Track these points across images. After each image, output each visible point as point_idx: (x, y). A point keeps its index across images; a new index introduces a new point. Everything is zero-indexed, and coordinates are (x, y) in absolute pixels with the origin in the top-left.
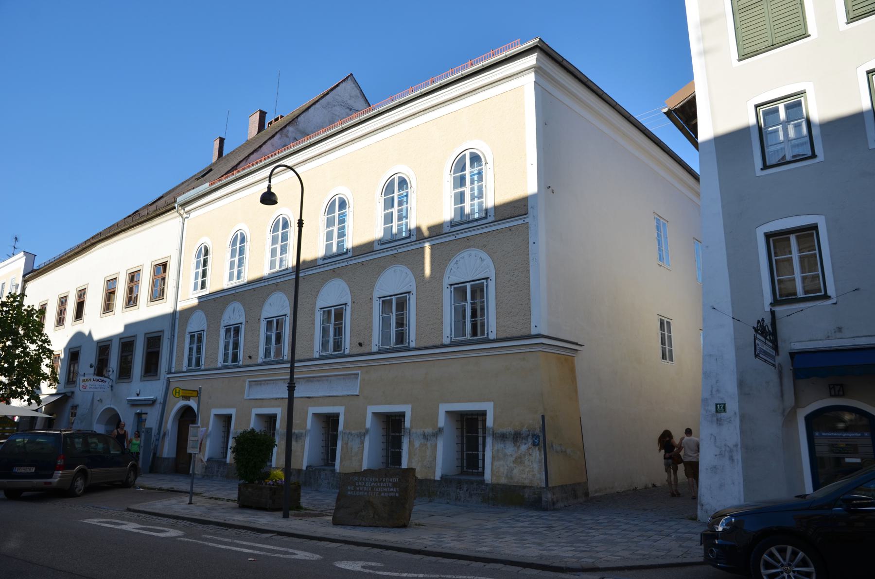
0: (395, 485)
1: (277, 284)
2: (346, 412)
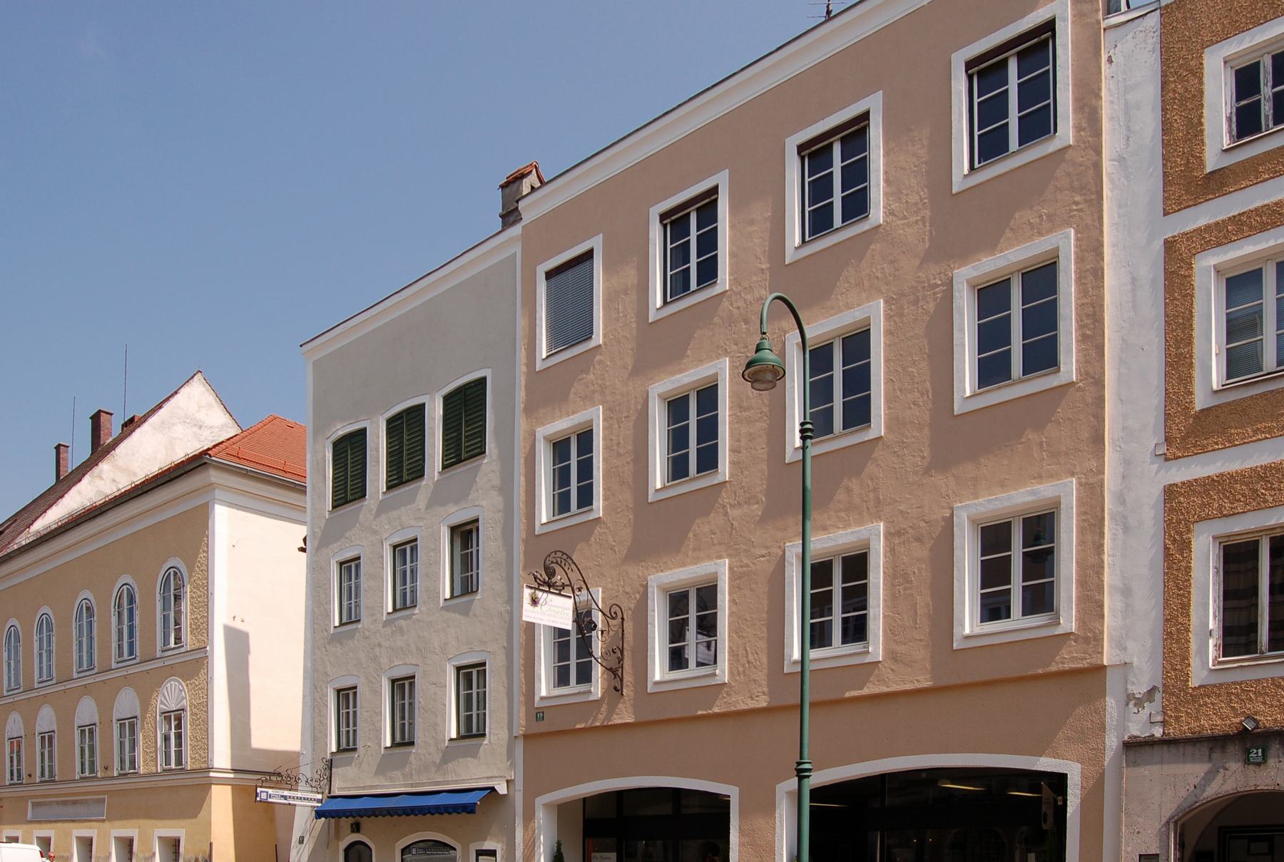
1: (45, 696)
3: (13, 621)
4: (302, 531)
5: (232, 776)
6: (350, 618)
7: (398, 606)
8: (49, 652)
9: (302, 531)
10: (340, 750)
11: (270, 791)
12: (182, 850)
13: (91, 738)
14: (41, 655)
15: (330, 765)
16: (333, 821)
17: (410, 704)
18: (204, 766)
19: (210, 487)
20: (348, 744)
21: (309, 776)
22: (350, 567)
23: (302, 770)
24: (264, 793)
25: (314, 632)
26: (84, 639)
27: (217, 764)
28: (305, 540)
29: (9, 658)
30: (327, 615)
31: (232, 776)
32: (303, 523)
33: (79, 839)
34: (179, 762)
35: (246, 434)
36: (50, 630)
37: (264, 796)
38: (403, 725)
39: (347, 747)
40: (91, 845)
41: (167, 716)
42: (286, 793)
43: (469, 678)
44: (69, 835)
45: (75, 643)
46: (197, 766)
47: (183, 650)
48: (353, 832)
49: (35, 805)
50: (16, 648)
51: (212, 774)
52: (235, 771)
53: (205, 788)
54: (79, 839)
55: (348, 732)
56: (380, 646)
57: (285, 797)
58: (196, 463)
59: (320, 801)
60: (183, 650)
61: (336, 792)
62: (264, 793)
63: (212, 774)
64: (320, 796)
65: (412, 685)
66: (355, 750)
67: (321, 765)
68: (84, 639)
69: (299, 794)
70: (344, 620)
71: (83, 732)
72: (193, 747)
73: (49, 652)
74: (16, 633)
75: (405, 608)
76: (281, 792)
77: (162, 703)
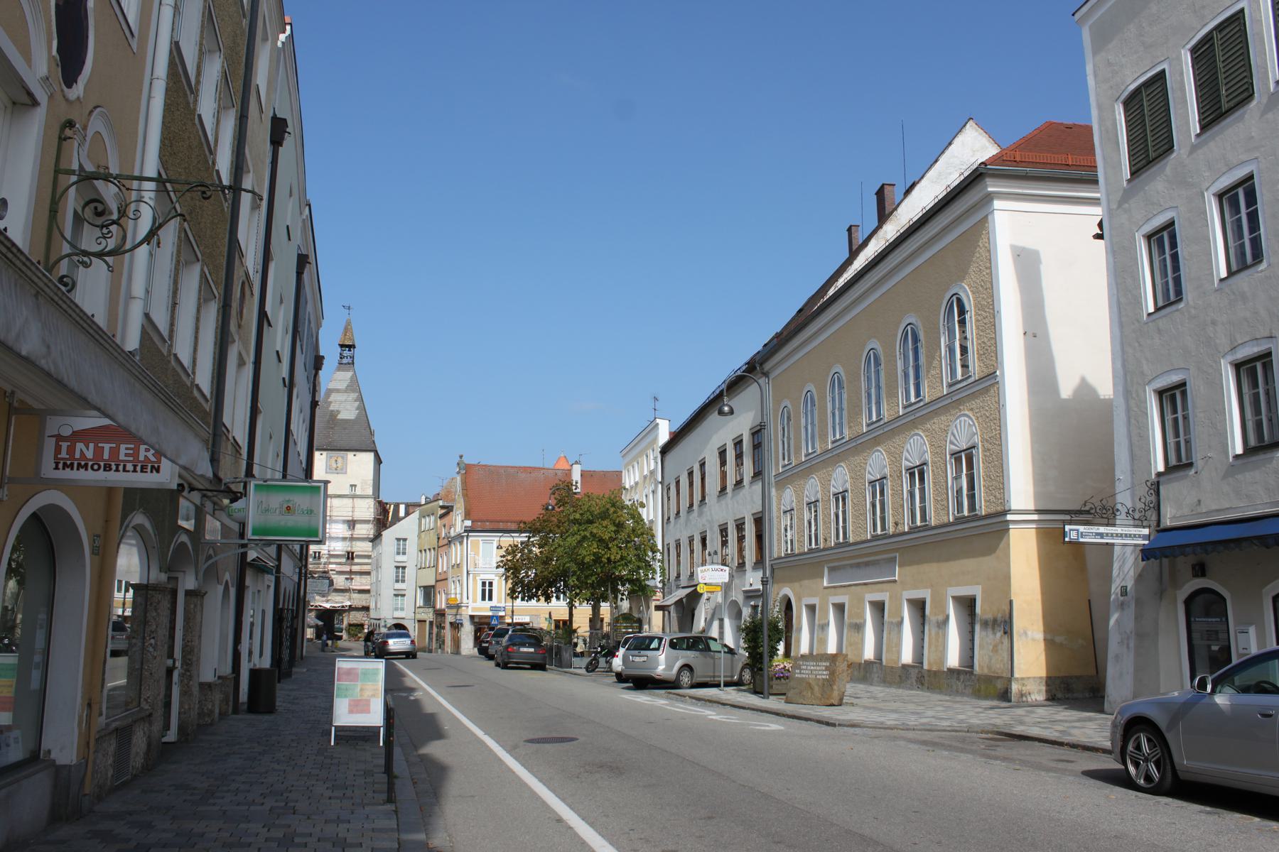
0: (827, 668)
2: (891, 597)
3: (787, 402)
4: (1096, 213)
5: (1035, 517)
6: (1171, 294)
7: (1234, 268)
8: (841, 409)
9: (1096, 213)
10: (1169, 469)
11: (1081, 528)
12: (978, 610)
13: (922, 479)
14: (834, 414)
15: (1156, 487)
16: (1165, 561)
17: (1267, 393)
18: (999, 509)
19: (989, 198)
20: (1179, 457)
21: (1129, 505)
22: (1164, 239)
23: (1119, 498)
24: (1075, 532)
25: (1121, 325)
26: (873, 390)
27: (1015, 504)
28: (1100, 225)
29: (834, 409)
30: (1137, 301)
31: (1035, 517)
32: (1094, 202)
33: (872, 603)
34: (972, 507)
35: (1003, 150)
36: (841, 387)
37: (1073, 535)
38: (1178, 444)
39: (1179, 465)
40: (923, 609)
41: (956, 456)
42: (1102, 529)
43: (1253, 375)
44: (861, 600)
45: (864, 395)
46: (992, 510)
47: (970, 381)
48: (1196, 575)
49: (831, 570)
50: (812, 411)
51: (1009, 517)
52: (1038, 512)
53: (1003, 530)
54: (872, 603)
55: (1178, 444)
56: (1214, 323)
57: (1101, 535)
58: (976, 177)
59: (1144, 537)
60: (970, 381)
61: (1167, 522)
62: (1075, 532)
63: (1009, 517)
64: (1146, 531)
65: (1184, 394)
66: (1190, 465)
67: (1143, 490)
68: (873, 390)
69: (1119, 530)
70: (1160, 304)
71: (912, 475)
72: (986, 487)
73: (841, 409)
74: (789, 413)
75: (1244, 267)
76: (1095, 529)
77: (951, 443)
